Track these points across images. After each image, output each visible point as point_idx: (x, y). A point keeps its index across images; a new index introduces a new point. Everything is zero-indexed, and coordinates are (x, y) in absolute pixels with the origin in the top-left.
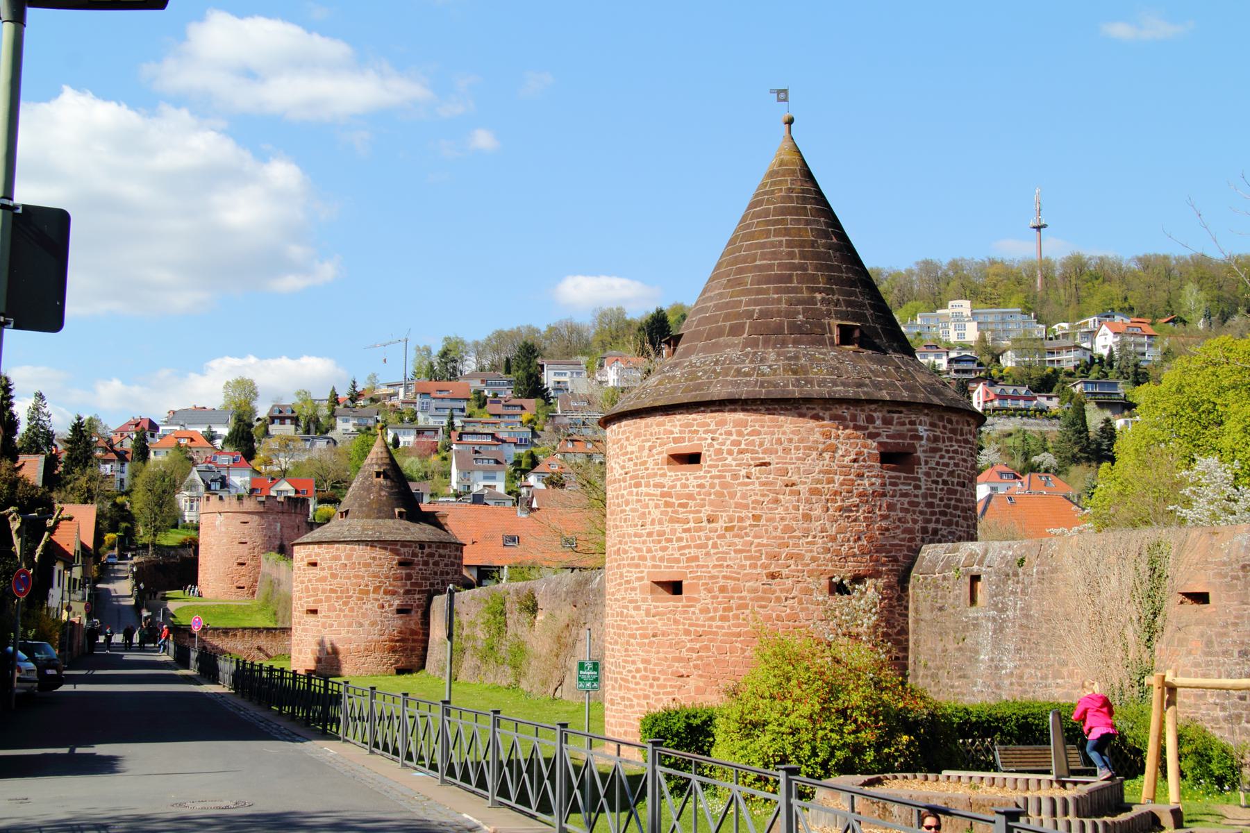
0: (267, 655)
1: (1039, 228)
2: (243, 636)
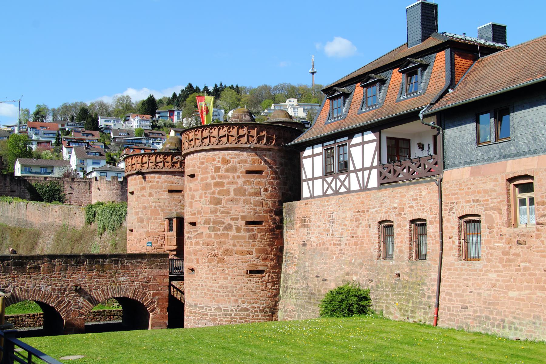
1: (313, 73)
2: (51, 269)
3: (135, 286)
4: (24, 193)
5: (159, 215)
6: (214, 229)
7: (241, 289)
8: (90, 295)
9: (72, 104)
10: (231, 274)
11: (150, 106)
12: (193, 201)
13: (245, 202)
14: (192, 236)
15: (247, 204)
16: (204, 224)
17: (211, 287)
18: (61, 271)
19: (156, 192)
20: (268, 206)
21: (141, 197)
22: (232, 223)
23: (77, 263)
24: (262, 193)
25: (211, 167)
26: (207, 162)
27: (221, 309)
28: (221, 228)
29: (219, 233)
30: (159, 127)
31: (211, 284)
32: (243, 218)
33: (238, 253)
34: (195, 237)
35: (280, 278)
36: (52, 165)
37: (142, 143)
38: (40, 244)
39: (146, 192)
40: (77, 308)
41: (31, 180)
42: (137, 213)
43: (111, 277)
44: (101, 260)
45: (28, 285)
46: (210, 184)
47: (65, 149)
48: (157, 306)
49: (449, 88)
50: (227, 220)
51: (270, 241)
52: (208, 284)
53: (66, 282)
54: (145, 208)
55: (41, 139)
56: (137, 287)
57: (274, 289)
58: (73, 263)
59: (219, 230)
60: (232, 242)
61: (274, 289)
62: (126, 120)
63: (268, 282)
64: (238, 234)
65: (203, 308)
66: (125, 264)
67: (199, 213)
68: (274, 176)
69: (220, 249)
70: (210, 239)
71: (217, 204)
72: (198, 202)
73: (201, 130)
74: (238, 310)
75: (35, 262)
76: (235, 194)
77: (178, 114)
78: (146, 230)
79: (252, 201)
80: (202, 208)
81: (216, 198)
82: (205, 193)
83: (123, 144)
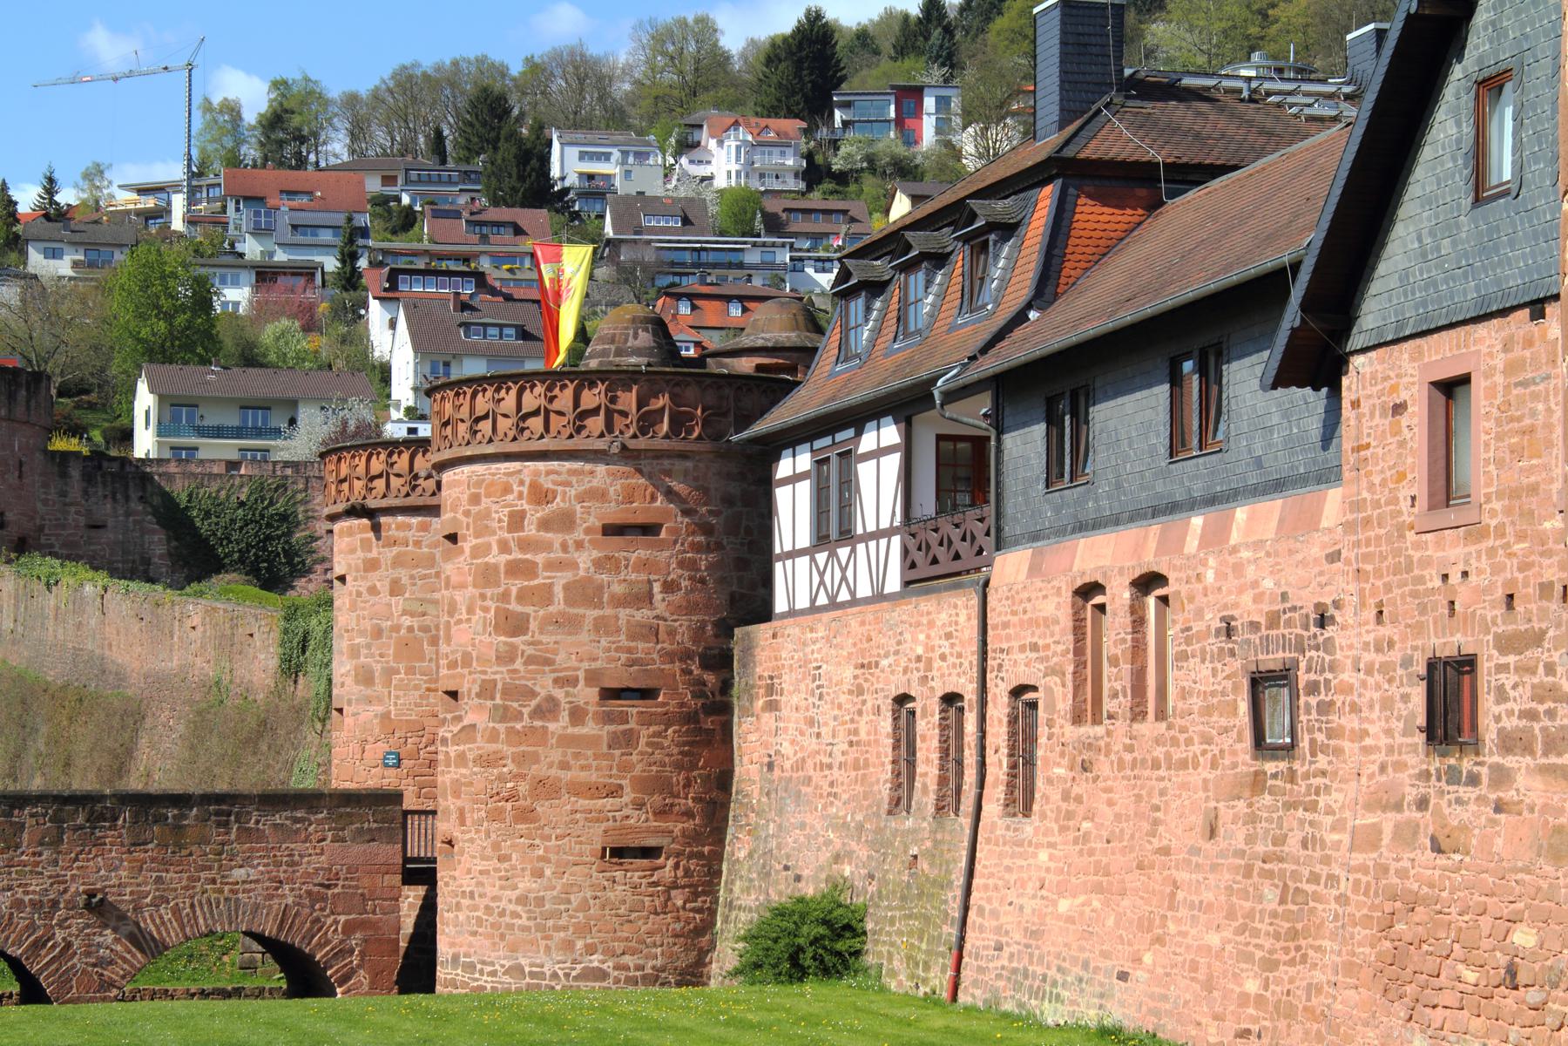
0: (139, 939)
3: (283, 896)
4: (143, 532)
5: (422, 659)
7: (584, 906)
8: (137, 924)
9: (438, 69)
10: (553, 857)
11: (810, 68)
12: (452, 621)
13: (600, 626)
14: (449, 735)
15: (607, 634)
16: (478, 695)
17: (495, 898)
18: (41, 844)
20: (678, 638)
21: (365, 595)
22: (559, 694)
23: (95, 819)
24: (658, 597)
26: (488, 495)
28: (526, 711)
29: (518, 726)
30: (842, 178)
31: (496, 891)
32: (592, 677)
33: (577, 790)
34: (457, 738)
35: (720, 872)
36: (291, 394)
37: (741, 266)
38: (144, 756)
39: (381, 580)
40: (94, 965)
41: (170, 477)
42: (354, 652)
43: (204, 868)
44: (171, 813)
46: (496, 567)
47: (374, 305)
48: (359, 966)
49: (1029, 306)
50: (545, 686)
51: (681, 753)
52: (489, 890)
53: (57, 879)
54: (378, 633)
55: (281, 256)
56: (290, 900)
57: (692, 910)
58: (80, 820)
60: (556, 755)
61: (692, 910)
62: (687, 146)
63: (674, 885)
64: (577, 730)
65: (470, 967)
66: (252, 824)
68: (700, 538)
69: (523, 776)
71: (514, 635)
73: (469, 391)
74: (574, 973)
76: (569, 601)
77: (943, 103)
78: (380, 709)
79: (622, 622)
80: (473, 645)
82: (483, 597)
83: (652, 272)
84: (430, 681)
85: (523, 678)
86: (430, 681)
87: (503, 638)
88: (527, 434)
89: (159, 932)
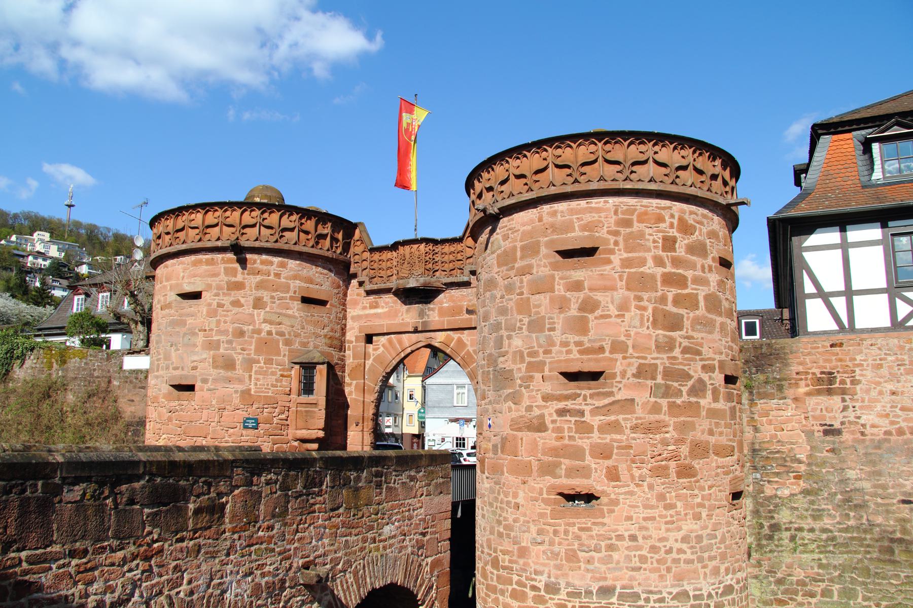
1: (70, 206)
5: (279, 354)
6: (667, 392)
10: (707, 503)
18: (273, 516)
19: (272, 297)
22: (705, 377)
25: (653, 236)
27: (689, 596)
28: (684, 390)
31: (662, 533)
39: (246, 297)
45: (190, 582)
46: (653, 277)
52: (655, 534)
59: (679, 393)
67: (618, 347)
70: (657, 417)
72: (613, 320)
74: (720, 591)
75: (209, 485)
78: (240, 387)
81: (670, 313)
82: (640, 299)
84: (283, 370)
85: (681, 364)
86: (283, 370)
87: (660, 332)
88: (208, 236)
89: (346, 598)
